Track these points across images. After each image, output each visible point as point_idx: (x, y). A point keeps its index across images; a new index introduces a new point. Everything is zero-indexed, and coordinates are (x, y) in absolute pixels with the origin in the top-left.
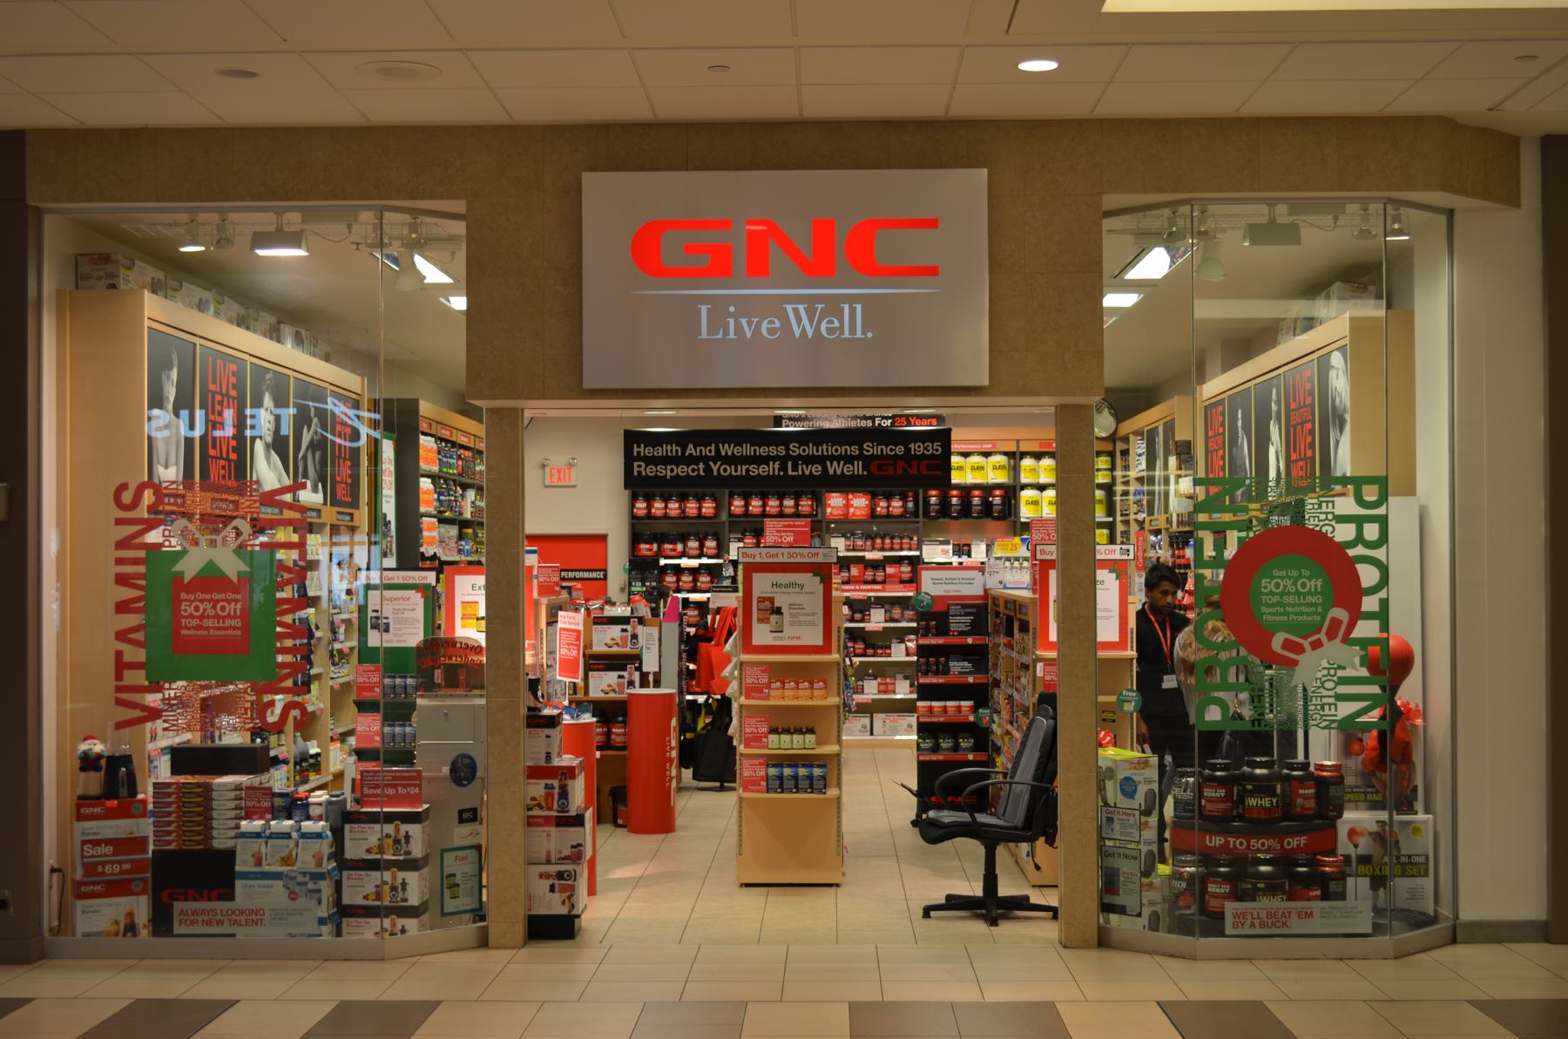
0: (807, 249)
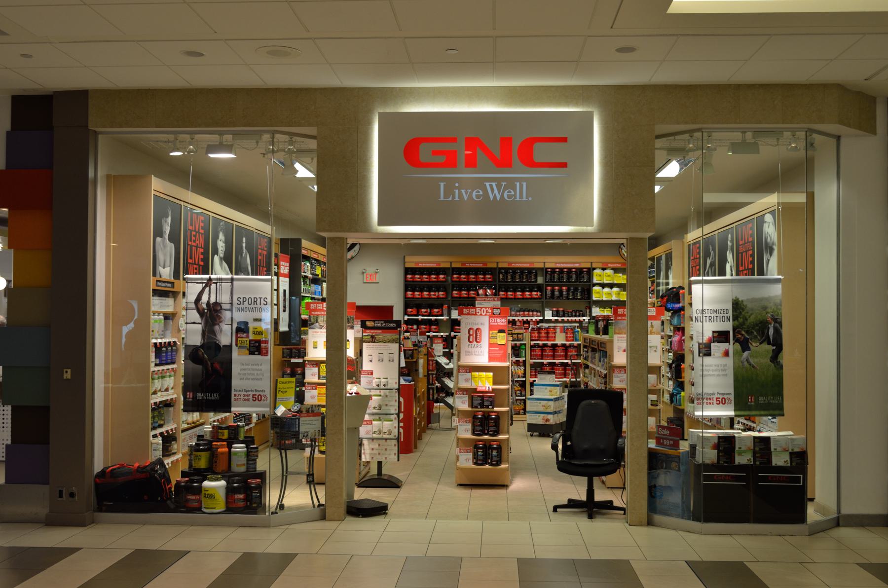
0: (497, 153)
